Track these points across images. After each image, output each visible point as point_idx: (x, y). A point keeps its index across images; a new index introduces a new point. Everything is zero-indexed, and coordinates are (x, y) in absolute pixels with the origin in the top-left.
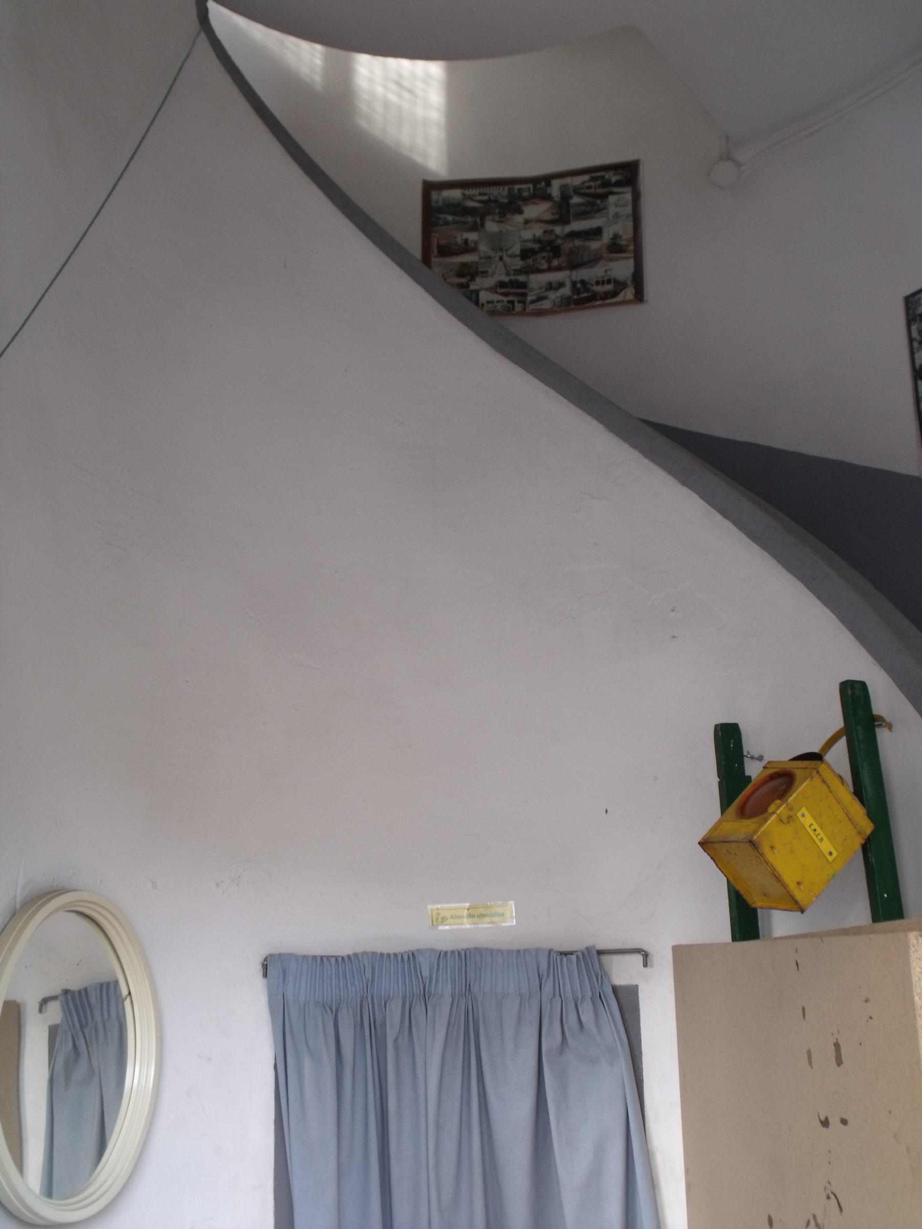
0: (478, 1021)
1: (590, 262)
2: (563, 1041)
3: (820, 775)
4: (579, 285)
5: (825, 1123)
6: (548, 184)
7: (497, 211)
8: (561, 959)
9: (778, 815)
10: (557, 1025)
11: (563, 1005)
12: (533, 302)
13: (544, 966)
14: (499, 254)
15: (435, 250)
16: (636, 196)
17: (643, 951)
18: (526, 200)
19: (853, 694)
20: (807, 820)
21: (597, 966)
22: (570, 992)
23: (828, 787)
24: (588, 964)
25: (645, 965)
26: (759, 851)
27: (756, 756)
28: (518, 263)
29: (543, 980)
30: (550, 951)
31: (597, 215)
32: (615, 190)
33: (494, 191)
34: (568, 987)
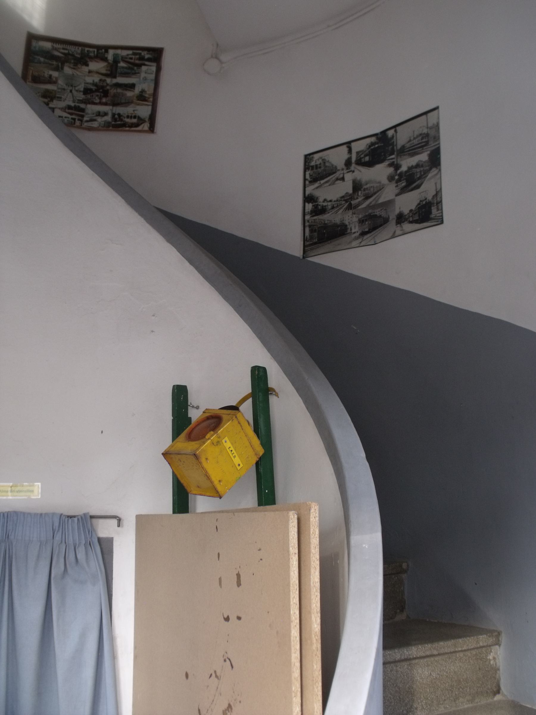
0: (12, 558)
1: (125, 103)
2: (65, 570)
3: (237, 419)
4: (116, 116)
5: (227, 619)
6: (106, 51)
7: (72, 61)
8: (68, 520)
9: (211, 440)
10: (62, 560)
11: (67, 548)
12: (87, 121)
13: (56, 524)
14: (70, 88)
15: (30, 78)
16: (159, 70)
17: (118, 517)
18: (91, 58)
19: (258, 374)
20: (228, 444)
21: (89, 525)
22: (72, 540)
23: (241, 426)
24: (84, 523)
25: (119, 526)
26: (199, 460)
27: (195, 406)
28: (81, 96)
29: (55, 533)
30: (61, 515)
31: (134, 76)
32: (147, 63)
33: (72, 49)
34: (71, 538)
